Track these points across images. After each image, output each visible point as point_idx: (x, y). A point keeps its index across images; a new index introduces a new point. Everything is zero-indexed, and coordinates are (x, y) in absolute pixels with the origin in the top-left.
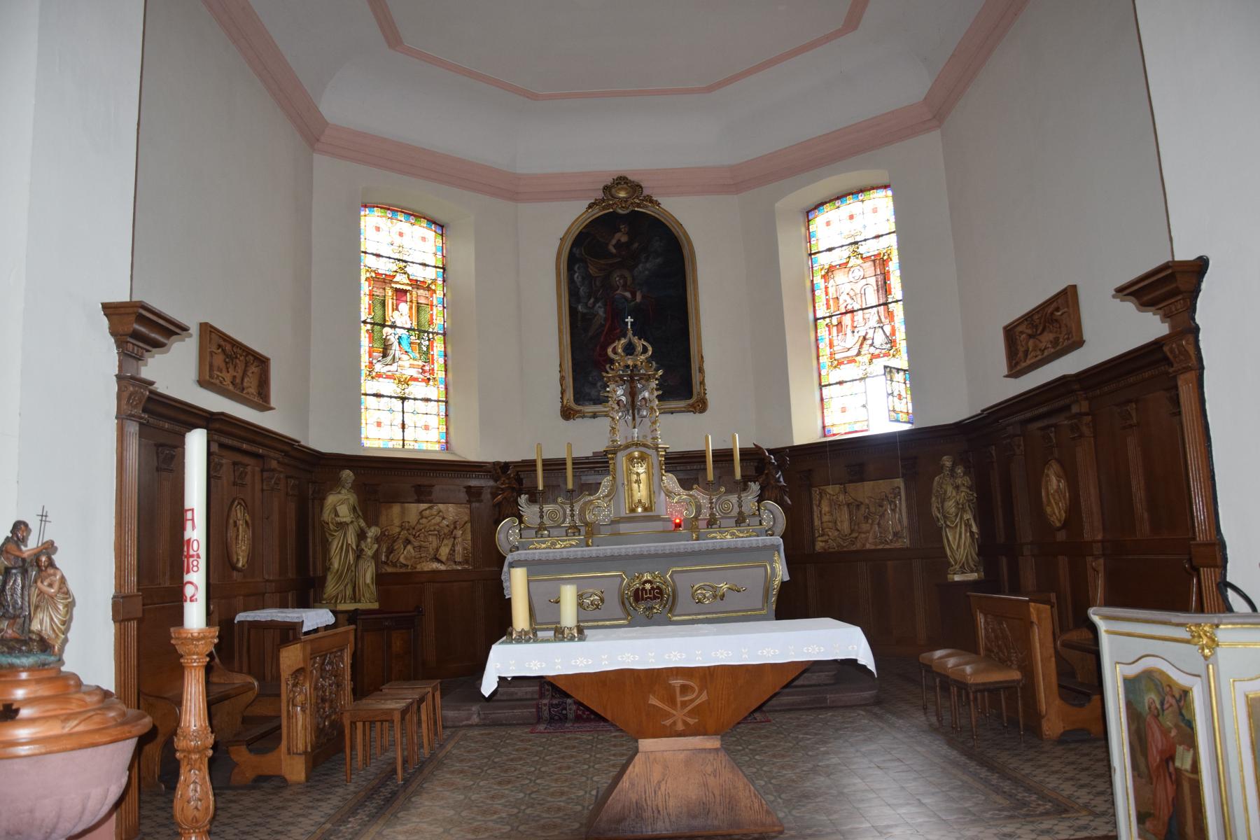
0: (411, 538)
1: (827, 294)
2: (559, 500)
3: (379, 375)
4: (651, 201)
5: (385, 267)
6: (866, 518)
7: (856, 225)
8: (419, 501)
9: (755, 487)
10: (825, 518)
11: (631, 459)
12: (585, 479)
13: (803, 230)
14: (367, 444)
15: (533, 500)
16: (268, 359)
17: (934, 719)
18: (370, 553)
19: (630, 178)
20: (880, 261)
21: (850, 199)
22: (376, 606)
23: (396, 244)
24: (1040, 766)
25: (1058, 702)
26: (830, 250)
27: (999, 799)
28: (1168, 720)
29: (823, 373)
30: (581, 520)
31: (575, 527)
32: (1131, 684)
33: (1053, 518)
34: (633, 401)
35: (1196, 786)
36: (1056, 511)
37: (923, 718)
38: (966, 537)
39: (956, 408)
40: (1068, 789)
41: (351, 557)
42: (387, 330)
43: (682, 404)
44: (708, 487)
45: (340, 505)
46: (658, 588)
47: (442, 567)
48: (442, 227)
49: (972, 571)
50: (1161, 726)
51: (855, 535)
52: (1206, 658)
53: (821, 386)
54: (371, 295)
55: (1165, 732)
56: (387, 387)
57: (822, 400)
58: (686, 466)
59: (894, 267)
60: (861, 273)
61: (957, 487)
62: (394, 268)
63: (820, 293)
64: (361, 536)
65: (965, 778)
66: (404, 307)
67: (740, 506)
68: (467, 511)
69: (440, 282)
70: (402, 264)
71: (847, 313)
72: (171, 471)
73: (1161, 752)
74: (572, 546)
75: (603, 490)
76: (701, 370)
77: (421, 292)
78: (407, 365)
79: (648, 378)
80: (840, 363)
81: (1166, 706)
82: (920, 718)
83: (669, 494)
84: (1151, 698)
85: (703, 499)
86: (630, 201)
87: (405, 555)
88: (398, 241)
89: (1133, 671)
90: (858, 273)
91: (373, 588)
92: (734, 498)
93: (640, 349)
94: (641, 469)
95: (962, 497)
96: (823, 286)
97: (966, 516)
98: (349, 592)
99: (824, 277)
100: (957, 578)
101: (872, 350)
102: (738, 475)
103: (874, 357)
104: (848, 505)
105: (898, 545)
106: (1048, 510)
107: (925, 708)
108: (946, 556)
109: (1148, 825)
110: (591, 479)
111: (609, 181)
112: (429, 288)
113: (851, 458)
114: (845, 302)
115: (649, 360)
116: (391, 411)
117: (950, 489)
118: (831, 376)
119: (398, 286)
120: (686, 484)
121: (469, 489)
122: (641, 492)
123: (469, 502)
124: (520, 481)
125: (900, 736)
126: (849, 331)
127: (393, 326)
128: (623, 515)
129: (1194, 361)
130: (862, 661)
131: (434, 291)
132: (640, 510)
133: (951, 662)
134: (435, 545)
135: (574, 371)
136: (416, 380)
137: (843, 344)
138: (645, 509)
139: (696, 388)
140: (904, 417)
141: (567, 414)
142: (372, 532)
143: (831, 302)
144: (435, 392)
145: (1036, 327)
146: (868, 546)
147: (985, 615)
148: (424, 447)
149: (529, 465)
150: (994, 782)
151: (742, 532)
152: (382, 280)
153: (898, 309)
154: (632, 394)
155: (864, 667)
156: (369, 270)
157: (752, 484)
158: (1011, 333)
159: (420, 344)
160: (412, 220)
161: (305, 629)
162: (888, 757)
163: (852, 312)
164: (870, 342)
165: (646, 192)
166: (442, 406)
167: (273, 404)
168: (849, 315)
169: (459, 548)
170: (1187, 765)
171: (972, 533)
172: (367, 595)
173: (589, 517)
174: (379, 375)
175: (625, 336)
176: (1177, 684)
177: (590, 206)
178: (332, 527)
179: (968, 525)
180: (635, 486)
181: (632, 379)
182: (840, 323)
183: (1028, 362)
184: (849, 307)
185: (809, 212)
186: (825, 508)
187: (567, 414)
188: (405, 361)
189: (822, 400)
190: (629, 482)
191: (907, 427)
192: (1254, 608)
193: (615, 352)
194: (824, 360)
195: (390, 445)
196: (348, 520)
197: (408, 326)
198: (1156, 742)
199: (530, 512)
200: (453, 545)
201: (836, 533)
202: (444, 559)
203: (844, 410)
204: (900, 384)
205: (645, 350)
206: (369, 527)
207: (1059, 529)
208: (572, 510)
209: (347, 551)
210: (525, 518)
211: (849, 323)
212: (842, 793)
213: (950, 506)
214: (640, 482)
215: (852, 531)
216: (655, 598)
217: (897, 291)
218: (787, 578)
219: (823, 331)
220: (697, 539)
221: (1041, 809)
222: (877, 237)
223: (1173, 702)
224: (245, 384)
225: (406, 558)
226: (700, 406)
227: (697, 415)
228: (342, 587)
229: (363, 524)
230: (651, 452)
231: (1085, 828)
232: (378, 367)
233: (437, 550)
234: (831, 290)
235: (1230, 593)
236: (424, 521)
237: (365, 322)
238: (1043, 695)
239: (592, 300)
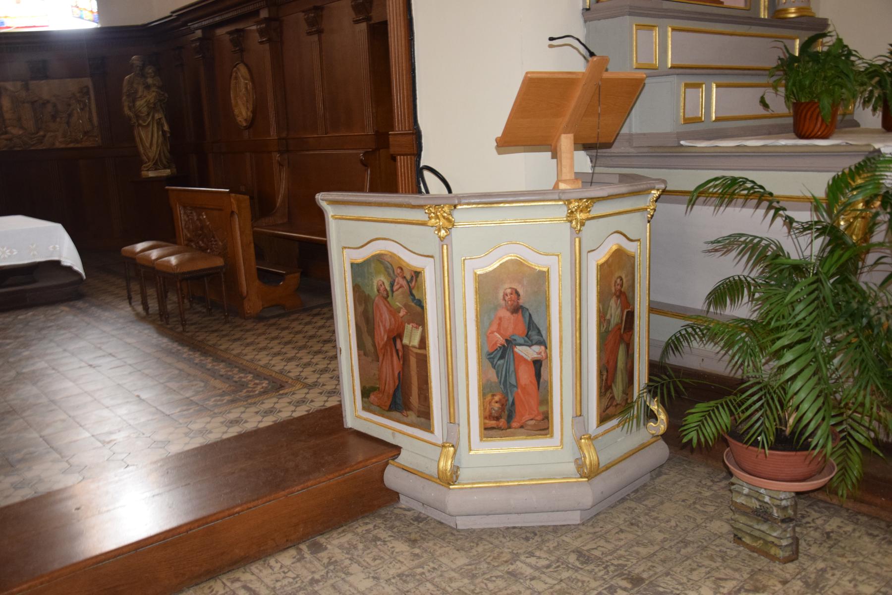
6: (54, 117)
17: (140, 309)
24: (248, 345)
25: (257, 283)
27: (217, 383)
28: (398, 300)
32: (358, 269)
33: (239, 119)
35: (423, 361)
36: (242, 112)
37: (130, 309)
38: (157, 137)
40: (278, 364)
49: (165, 168)
50: (389, 306)
51: (41, 133)
52: (442, 239)
55: (394, 312)
61: (148, 87)
65: (181, 365)
73: (389, 331)
81: (395, 288)
82: (125, 310)
84: (380, 280)
89: (361, 256)
95: (151, 96)
97: (157, 116)
100: (151, 174)
106: (236, 112)
107: (130, 299)
109: (372, 397)
117: (141, 89)
125: (107, 328)
130: (66, 262)
133: (154, 254)
140: (90, 16)
146: (58, 145)
147: (185, 207)
150: (209, 366)
155: (69, 269)
162: (100, 353)
170: (416, 342)
171: (164, 132)
176: (408, 265)
179: (160, 124)
192: (450, 191)
198: (384, 322)
207: (247, 128)
212: (53, 402)
221: (259, 389)
223: (404, 283)
231: (302, 401)
235: (427, 174)
238: (243, 278)
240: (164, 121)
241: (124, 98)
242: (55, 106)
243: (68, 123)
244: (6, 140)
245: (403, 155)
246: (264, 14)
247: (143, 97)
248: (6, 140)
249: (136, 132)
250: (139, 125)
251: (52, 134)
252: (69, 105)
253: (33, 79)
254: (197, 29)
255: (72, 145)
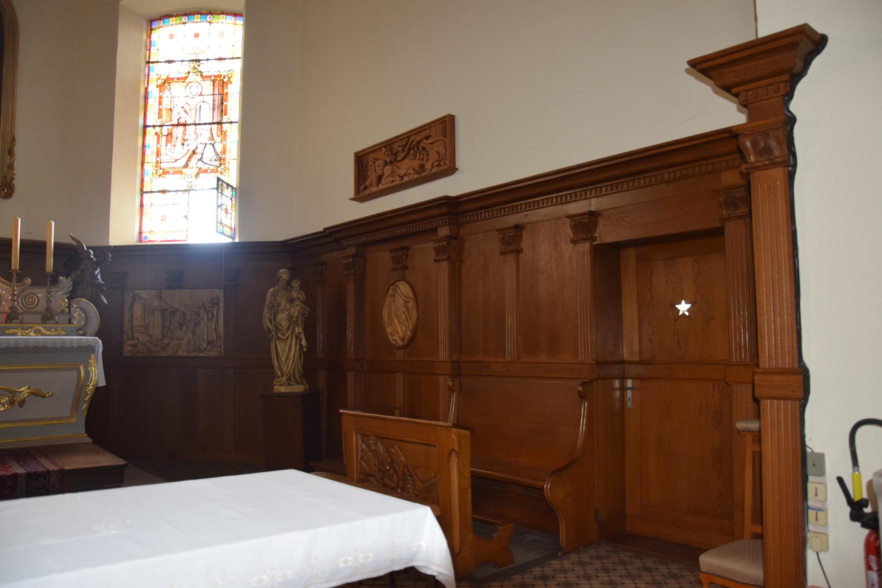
1: (160, 104)
6: (181, 326)
13: (145, 36)
20: (220, 83)
21: (197, 18)
29: (147, 179)
49: (297, 383)
51: (166, 341)
53: (142, 192)
57: (142, 205)
59: (234, 91)
61: (291, 301)
71: (178, 125)
80: (165, 173)
90: (195, 90)
92: (41, 293)
95: (296, 310)
100: (283, 389)
101: (200, 164)
103: (201, 171)
105: (212, 354)
106: (389, 330)
117: (283, 302)
118: (153, 183)
126: (179, 143)
129: (792, 162)
137: (170, 154)
140: (228, 232)
143: (164, 112)
145: (395, 155)
146: (181, 353)
151: (49, 329)
153: (233, 133)
158: (361, 160)
163: (185, 125)
164: (199, 156)
168: (181, 128)
179: (298, 338)
182: (170, 134)
183: (381, 187)
184: (182, 121)
185: (151, 22)
189: (142, 205)
194: (149, 168)
201: (147, 338)
203: (163, 218)
204: (228, 199)
207: (400, 348)
211: (180, 136)
215: (164, 337)
218: (102, 383)
222: (220, 59)
240: (303, 336)
241: (266, 310)
242: (184, 314)
243: (194, 332)
244: (131, 345)
245: (778, 399)
246: (444, 231)
247: (284, 311)
248: (131, 345)
249: (273, 346)
250: (278, 338)
251: (176, 342)
252: (198, 315)
253: (168, 288)
254: (350, 246)
255: (194, 354)
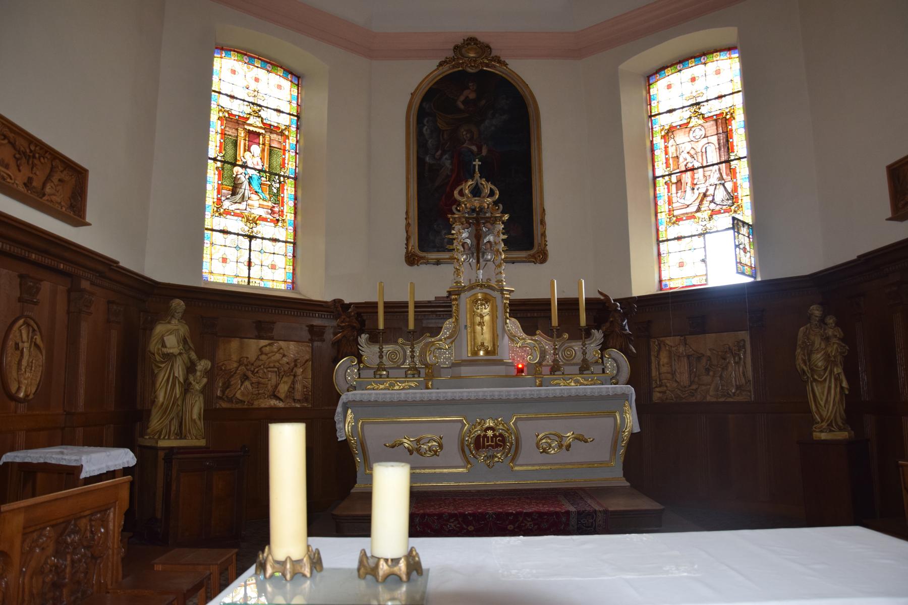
0: (249, 374)
2: (400, 340)
3: (228, 212)
4: (499, 62)
5: (238, 108)
6: (708, 370)
7: (699, 85)
8: (260, 337)
9: (598, 335)
10: (664, 369)
11: (475, 301)
12: (425, 323)
13: (644, 93)
14: (212, 279)
15: (374, 338)
16: (86, 171)
18: (198, 387)
19: (481, 39)
20: (723, 121)
21: (692, 62)
22: (202, 443)
23: (252, 88)
26: (670, 111)
30: (421, 362)
31: (416, 369)
34: (478, 244)
39: (808, 259)
41: (178, 391)
42: (236, 169)
43: (523, 254)
44: (549, 332)
45: (170, 336)
46: (501, 435)
47: (281, 405)
48: (298, 77)
49: (840, 430)
51: (694, 387)
54: (223, 134)
56: (235, 224)
58: (529, 313)
60: (703, 132)
61: (827, 339)
62: (248, 110)
63: (660, 155)
64: (191, 369)
66: (256, 149)
67: (584, 353)
68: (309, 350)
69: (293, 129)
70: (256, 108)
71: (686, 171)
72: (36, 304)
74: (411, 388)
75: (445, 333)
76: (543, 222)
77: (274, 136)
78: (257, 205)
79: (493, 221)
80: (679, 219)
83: (512, 338)
85: (548, 345)
86: (480, 60)
87: (241, 390)
88: (253, 85)
90: (699, 133)
91: (200, 424)
92: (577, 346)
93: (487, 191)
94: (486, 310)
96: (662, 146)
98: (174, 427)
99: (663, 137)
100: (824, 436)
101: (713, 206)
102: (583, 321)
103: (714, 213)
104: (688, 357)
108: (810, 412)
110: (432, 323)
111: (460, 41)
112: (282, 134)
113: (691, 308)
114: (685, 160)
115: (496, 203)
116: (237, 248)
117: (817, 341)
119: (251, 128)
120: (529, 330)
121: (311, 328)
122: (485, 335)
123: (311, 341)
124: (363, 323)
126: (688, 189)
127: (244, 166)
128: (464, 358)
131: (287, 137)
132: (482, 353)
134: (274, 382)
135: (419, 218)
136: (265, 220)
137: (682, 201)
138: (487, 353)
139: (537, 239)
140: (748, 270)
141: (411, 260)
142: (203, 365)
143: (671, 161)
144: (284, 233)
146: (709, 399)
148: (270, 285)
149: (371, 307)
152: (233, 120)
153: (743, 169)
154: (478, 237)
155: (353, 487)
156: (222, 109)
157: (594, 331)
159: (270, 186)
160: (269, 67)
161: (83, 475)
163: (692, 169)
164: (710, 198)
165: (494, 54)
166: (290, 247)
167: (88, 219)
168: (689, 173)
169: (298, 386)
171: (842, 388)
172: (194, 431)
173: (430, 359)
174: (228, 212)
175: (472, 177)
177: (441, 64)
178: (158, 358)
179: (837, 379)
180: (478, 328)
181: (477, 220)
182: (679, 182)
184: (690, 165)
186: (664, 359)
187: (411, 260)
188: (255, 201)
189: (659, 254)
190: (473, 324)
191: (751, 280)
193: (461, 193)
194: (663, 217)
195: (235, 281)
196: (175, 351)
197: (259, 167)
199: (369, 352)
200: (293, 383)
201: (675, 385)
202: (282, 396)
203: (681, 265)
205: (492, 194)
206: (200, 358)
208: (412, 352)
209: (174, 385)
210: (365, 358)
213: (818, 359)
214: (483, 324)
215: (692, 383)
216: (497, 446)
217: (740, 146)
218: (637, 429)
219: (661, 189)
220: (541, 385)
224: (48, 190)
225: (243, 394)
226: (541, 257)
227: (538, 266)
228: (167, 422)
229: (194, 356)
230: (496, 294)
232: (227, 204)
233: (276, 386)
234: (672, 150)
236: (263, 357)
237: (215, 159)
239: (439, 152)
240: (843, 377)
241: (799, 350)
242: (709, 359)
244: (660, 392)
249: (809, 388)
250: (815, 380)
252: (725, 359)
255: (722, 400)
